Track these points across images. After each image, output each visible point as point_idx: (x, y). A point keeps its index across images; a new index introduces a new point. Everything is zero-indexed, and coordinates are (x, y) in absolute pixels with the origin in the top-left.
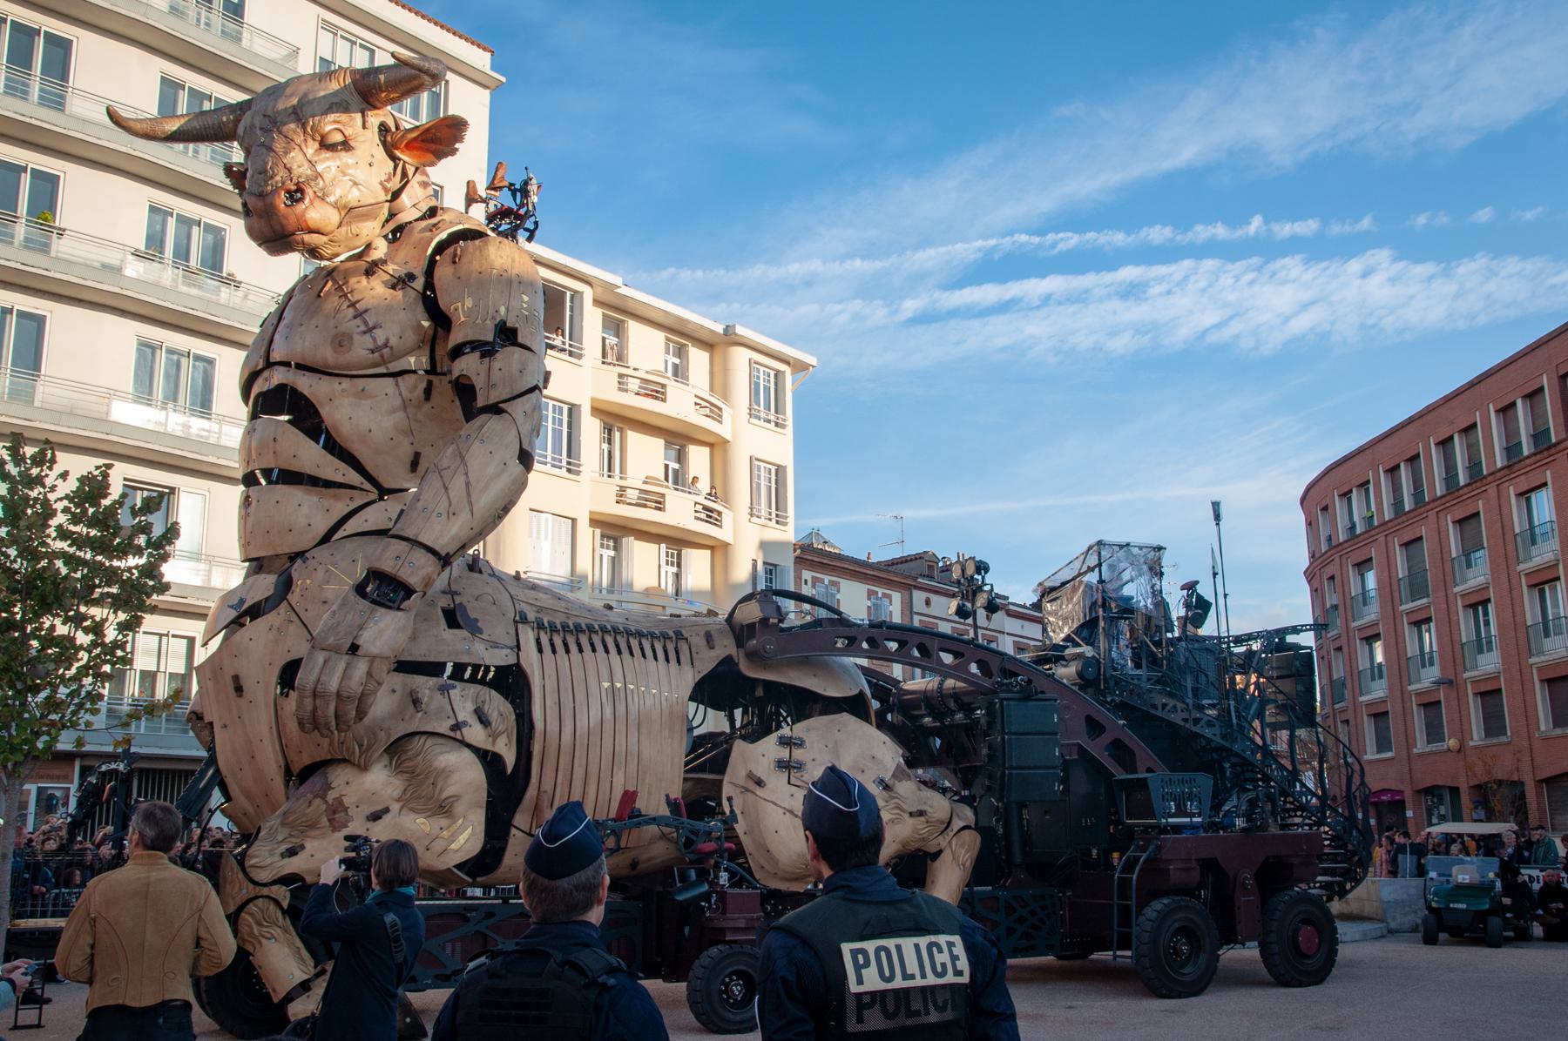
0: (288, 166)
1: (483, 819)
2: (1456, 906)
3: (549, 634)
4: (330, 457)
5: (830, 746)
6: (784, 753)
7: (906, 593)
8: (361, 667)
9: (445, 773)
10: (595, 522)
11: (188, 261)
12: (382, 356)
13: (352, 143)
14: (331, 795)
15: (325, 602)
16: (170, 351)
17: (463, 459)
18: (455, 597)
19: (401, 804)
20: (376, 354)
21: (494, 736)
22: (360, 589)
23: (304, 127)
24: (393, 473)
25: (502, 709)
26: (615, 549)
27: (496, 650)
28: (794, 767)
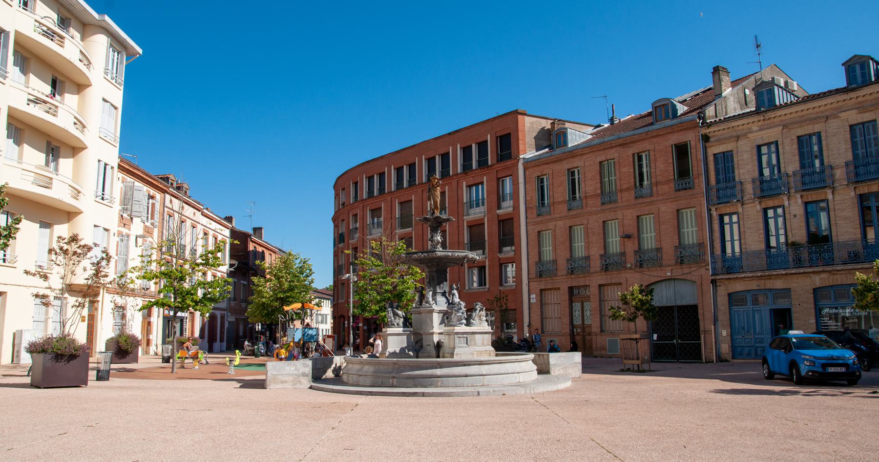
2: (795, 378)
7: (163, 194)
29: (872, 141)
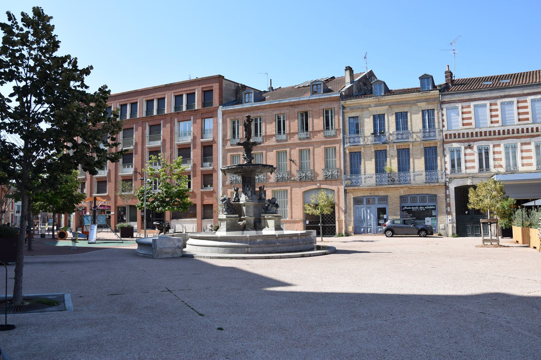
29: (432, 119)
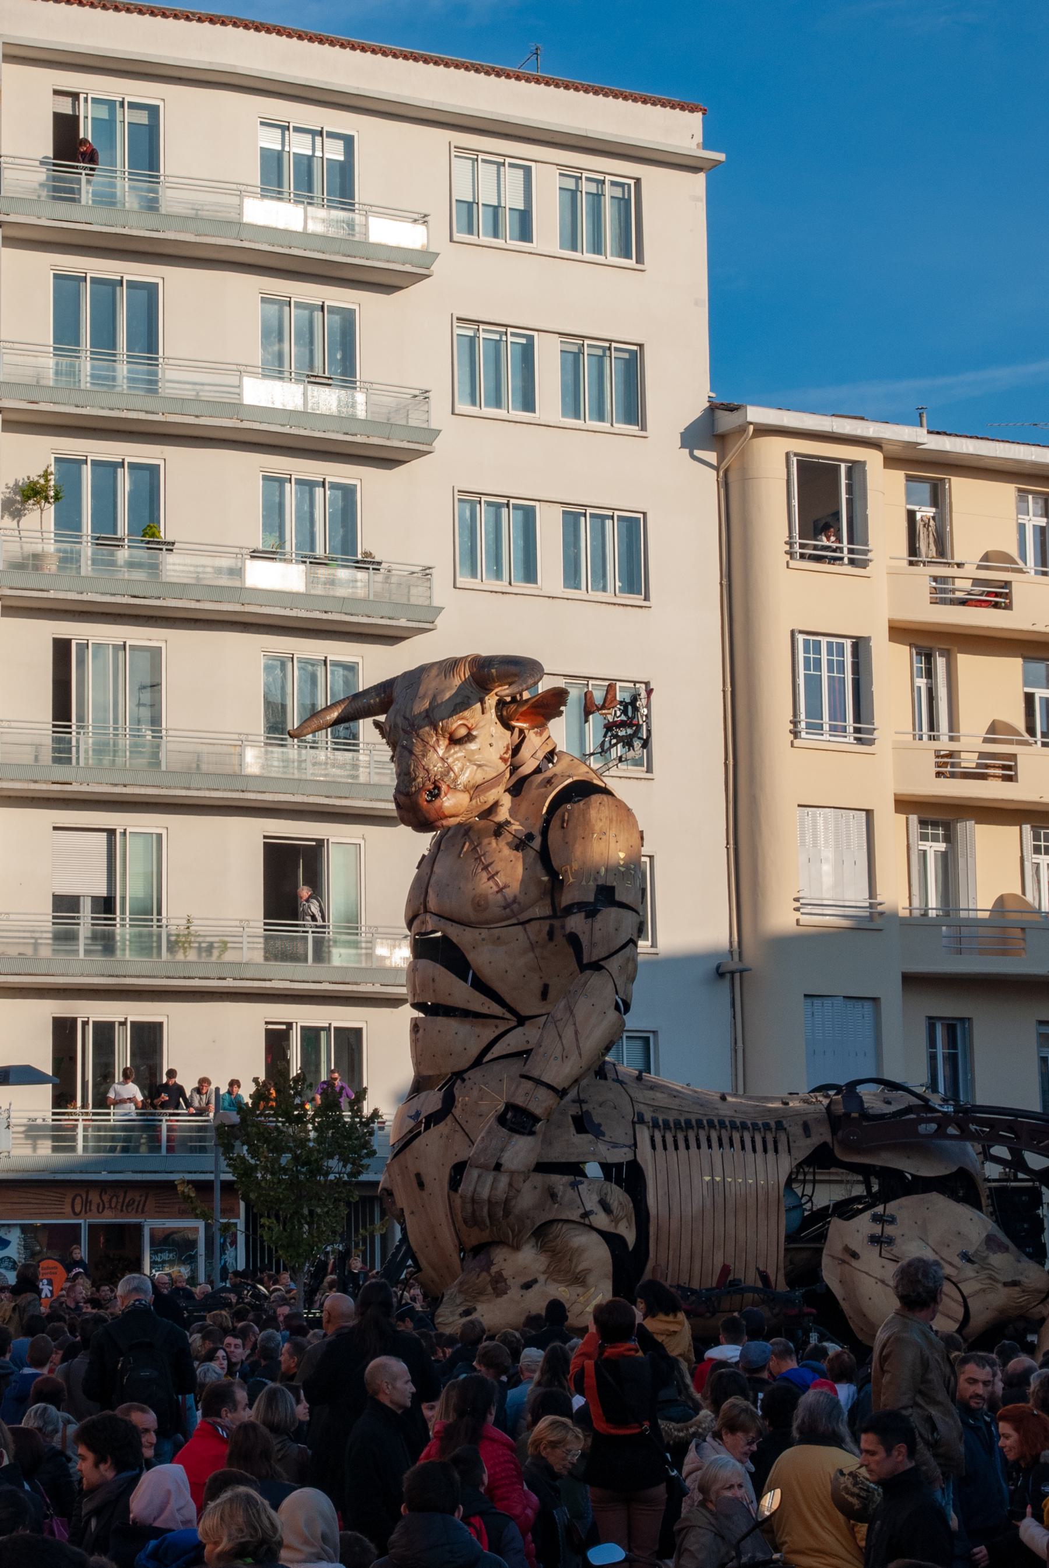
0: (426, 767)
1: (611, 1288)
3: (662, 1131)
4: (477, 993)
5: (919, 1223)
6: (877, 1229)
8: (504, 1180)
9: (579, 1251)
10: (904, 804)
11: (313, 549)
12: (512, 911)
13: (474, 733)
14: (494, 1270)
15: (481, 1115)
16: (305, 662)
17: (572, 1012)
18: (583, 1105)
19: (546, 1276)
20: (508, 910)
21: (616, 1221)
22: (501, 1120)
23: (436, 729)
24: (528, 1005)
25: (621, 1200)
26: (948, 839)
27: (616, 1150)
28: (885, 1242)
